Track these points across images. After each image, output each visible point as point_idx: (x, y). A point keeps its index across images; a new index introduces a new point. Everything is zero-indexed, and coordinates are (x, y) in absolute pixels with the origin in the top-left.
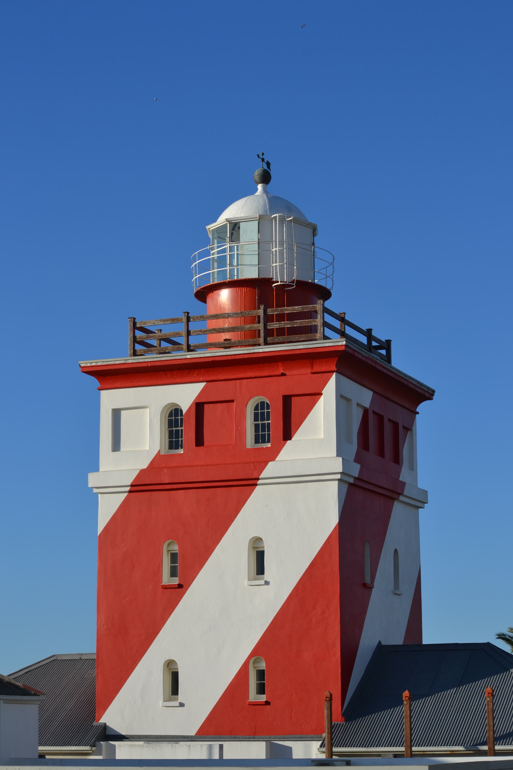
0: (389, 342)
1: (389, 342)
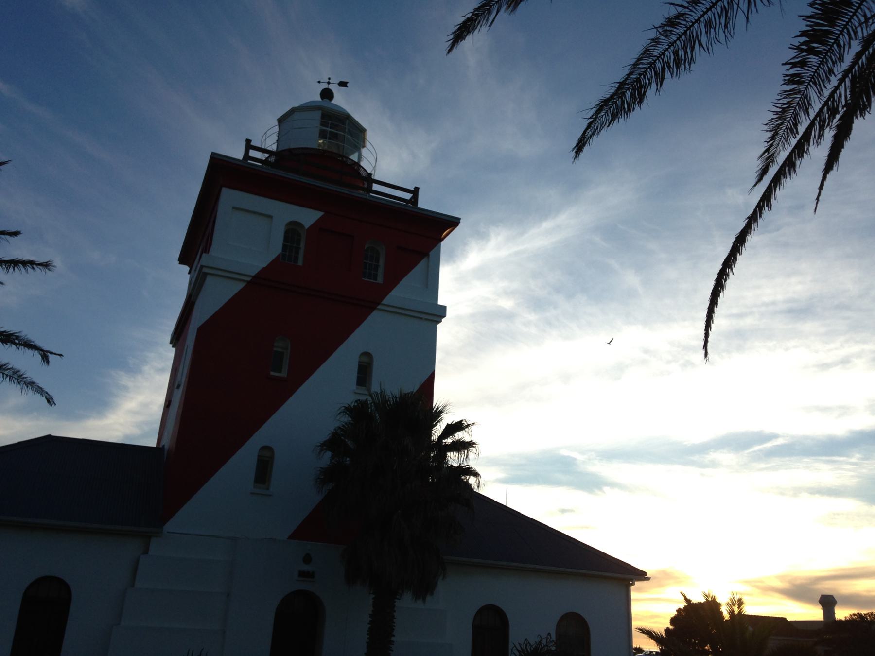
0: (417, 189)
1: (417, 189)
